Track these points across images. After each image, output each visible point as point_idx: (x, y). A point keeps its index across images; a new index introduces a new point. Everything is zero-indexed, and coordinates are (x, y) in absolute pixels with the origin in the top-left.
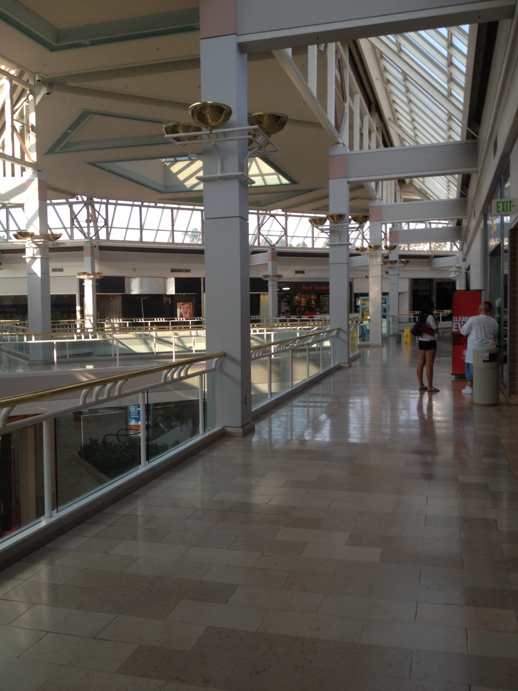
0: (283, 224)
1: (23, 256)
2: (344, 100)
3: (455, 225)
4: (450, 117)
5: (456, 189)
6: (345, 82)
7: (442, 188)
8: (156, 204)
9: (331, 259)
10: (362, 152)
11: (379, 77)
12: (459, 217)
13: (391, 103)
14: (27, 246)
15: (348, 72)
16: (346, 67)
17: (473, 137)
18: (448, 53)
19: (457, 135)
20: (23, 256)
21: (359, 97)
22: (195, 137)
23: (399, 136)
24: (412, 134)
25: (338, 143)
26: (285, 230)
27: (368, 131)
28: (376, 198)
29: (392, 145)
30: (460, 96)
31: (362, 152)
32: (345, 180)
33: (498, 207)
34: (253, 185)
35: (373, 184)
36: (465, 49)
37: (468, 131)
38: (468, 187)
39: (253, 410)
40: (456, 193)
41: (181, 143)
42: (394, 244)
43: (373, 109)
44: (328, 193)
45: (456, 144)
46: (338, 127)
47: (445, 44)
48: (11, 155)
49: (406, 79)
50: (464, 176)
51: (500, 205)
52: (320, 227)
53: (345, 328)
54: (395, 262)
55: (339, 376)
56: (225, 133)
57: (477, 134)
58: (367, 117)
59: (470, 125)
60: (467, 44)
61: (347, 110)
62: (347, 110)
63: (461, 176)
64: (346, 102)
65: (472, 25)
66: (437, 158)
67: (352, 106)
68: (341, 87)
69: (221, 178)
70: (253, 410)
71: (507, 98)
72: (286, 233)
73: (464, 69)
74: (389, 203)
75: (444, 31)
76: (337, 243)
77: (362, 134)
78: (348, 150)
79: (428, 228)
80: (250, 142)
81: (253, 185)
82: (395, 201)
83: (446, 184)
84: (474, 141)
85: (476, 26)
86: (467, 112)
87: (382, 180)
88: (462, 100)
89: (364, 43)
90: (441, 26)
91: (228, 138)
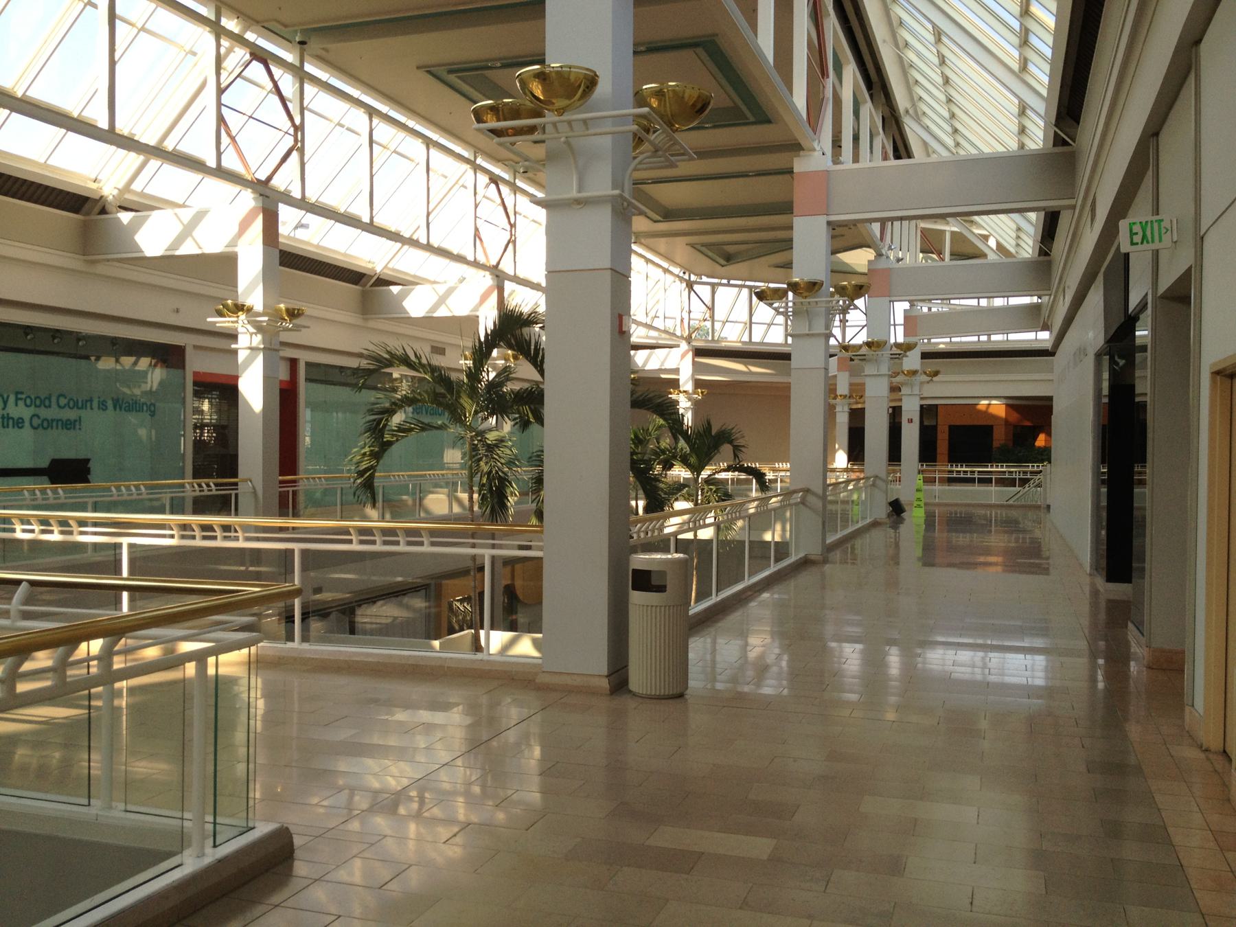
0: (708, 300)
1: (233, 346)
2: (824, 73)
4: (1022, 111)
7: (1008, 233)
9: (794, 362)
11: (888, 38)
13: (910, 84)
14: (240, 330)
15: (832, 22)
17: (1047, 254)
18: (1021, 24)
19: (1038, 137)
20: (233, 346)
21: (851, 71)
22: (531, 130)
23: (925, 144)
24: (949, 142)
26: (711, 309)
28: (814, 150)
30: (1042, 76)
32: (822, 221)
33: (1132, 234)
35: (876, 227)
36: (1051, 22)
38: (1077, 119)
39: (691, 613)
40: (1041, 134)
41: (502, 139)
42: (912, 340)
43: (877, 87)
45: (1037, 157)
46: (882, 239)
47: (1016, 41)
48: (299, 196)
49: (939, 40)
51: (1136, 229)
52: (776, 305)
54: (914, 373)
55: (806, 578)
56: (585, 121)
58: (867, 108)
59: (1058, 123)
60: (1054, 10)
61: (829, 93)
62: (829, 93)
66: (997, 181)
69: (578, 202)
70: (691, 613)
72: (712, 317)
73: (1048, 52)
77: (856, 138)
78: (830, 163)
79: (978, 306)
80: (638, 141)
83: (1014, 235)
84: (1047, 258)
87: (893, 219)
88: (1044, 93)
91: (591, 131)
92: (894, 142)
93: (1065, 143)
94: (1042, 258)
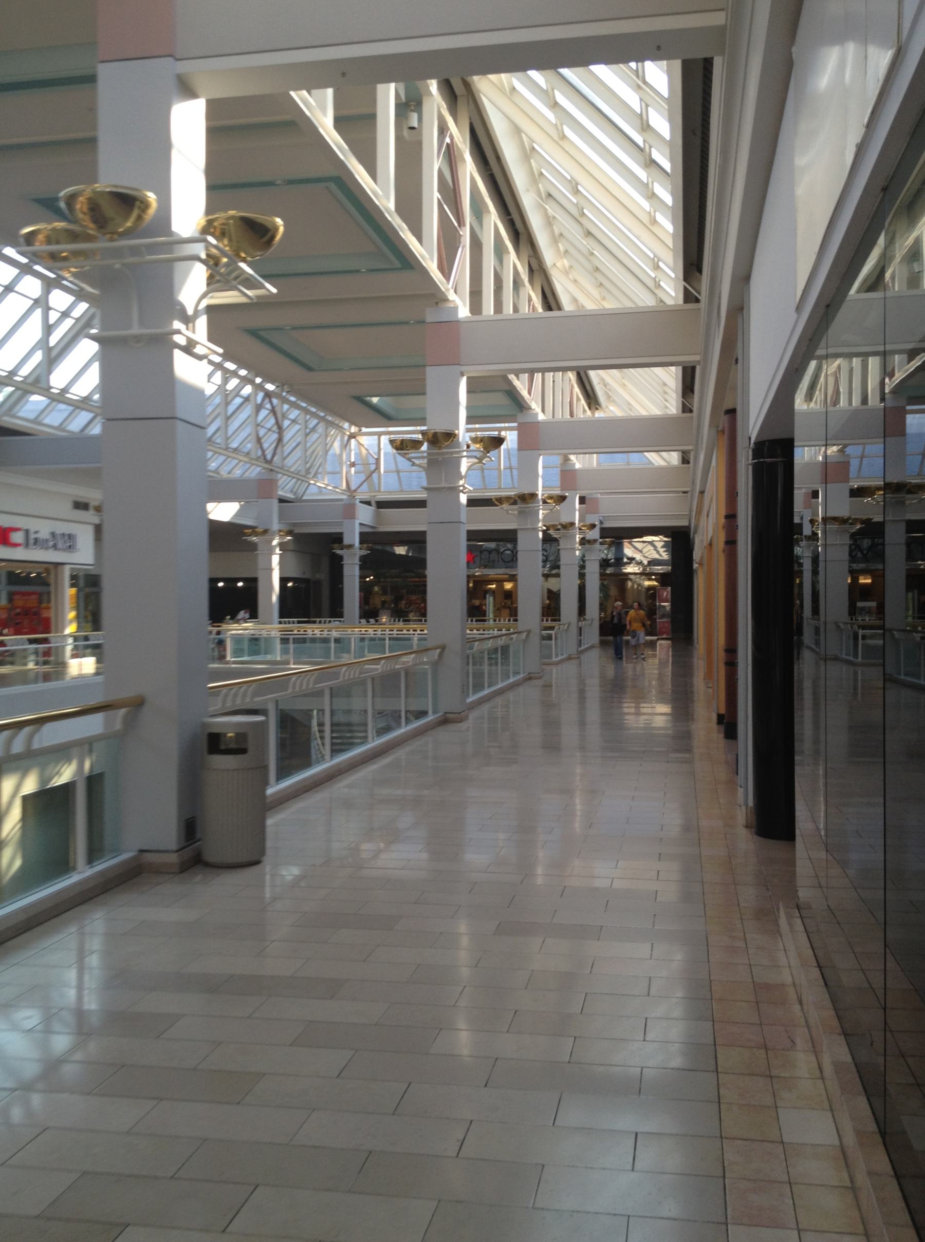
6: (463, 199)
10: (499, 317)
15: (469, 168)
16: (464, 161)
21: (493, 218)
29: (559, 308)
31: (499, 317)
43: (523, 238)
44: (376, 111)
50: (685, 370)
53: (429, 644)
63: (680, 368)
64: (464, 225)
65: (671, 61)
68: (451, 193)
71: (746, 65)
74: (559, 415)
75: (633, 65)
82: (572, 415)
85: (677, 64)
89: (592, 374)
90: (631, 61)
94: (685, 415)
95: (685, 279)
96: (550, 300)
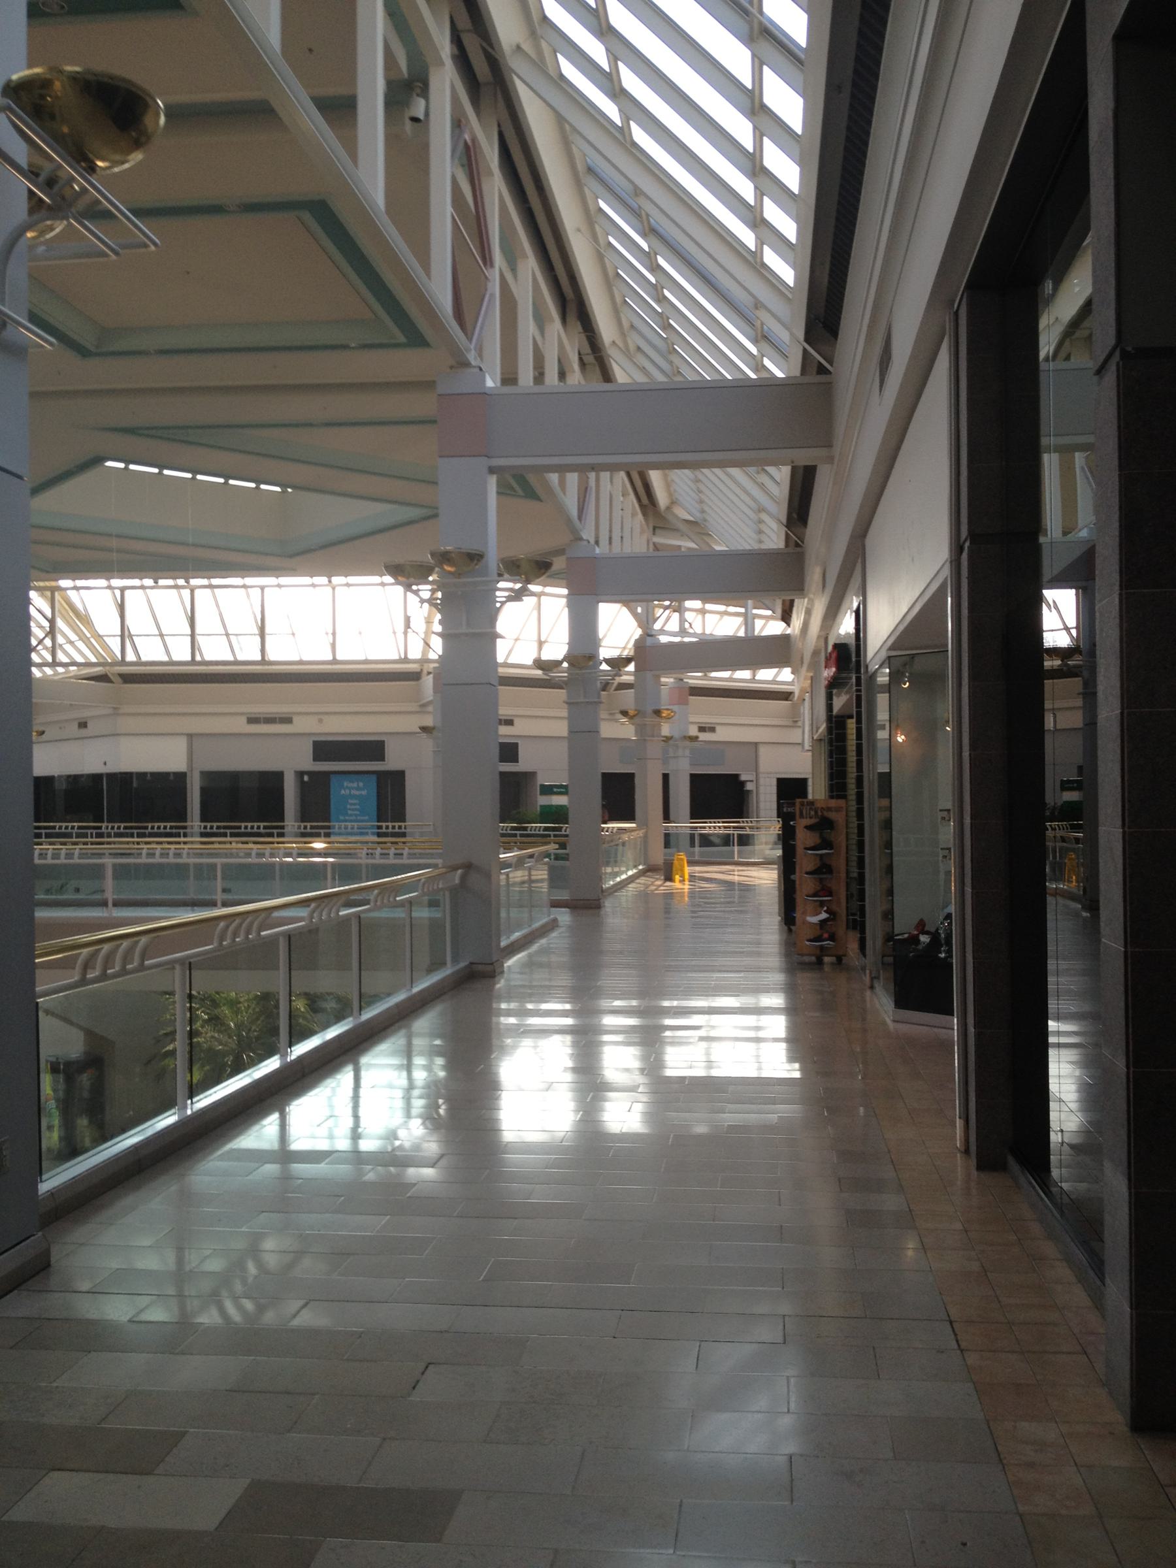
3: (796, 371)
5: (774, 525)
8: (156, 582)
12: (805, 457)
15: (496, 187)
16: (490, 173)
19: (774, 538)
21: (530, 265)
25: (581, 539)
27: (556, 371)
34: (817, 791)
37: (805, 350)
57: (831, 363)
59: (810, 336)
61: (495, 288)
62: (495, 288)
64: (492, 265)
67: (509, 277)
68: (473, 221)
76: (582, 699)
81: (817, 791)
84: (822, 378)
86: (812, 201)
89: (655, 476)
92: (501, 136)
93: (797, 545)
95: (807, 340)
96: (595, 357)
